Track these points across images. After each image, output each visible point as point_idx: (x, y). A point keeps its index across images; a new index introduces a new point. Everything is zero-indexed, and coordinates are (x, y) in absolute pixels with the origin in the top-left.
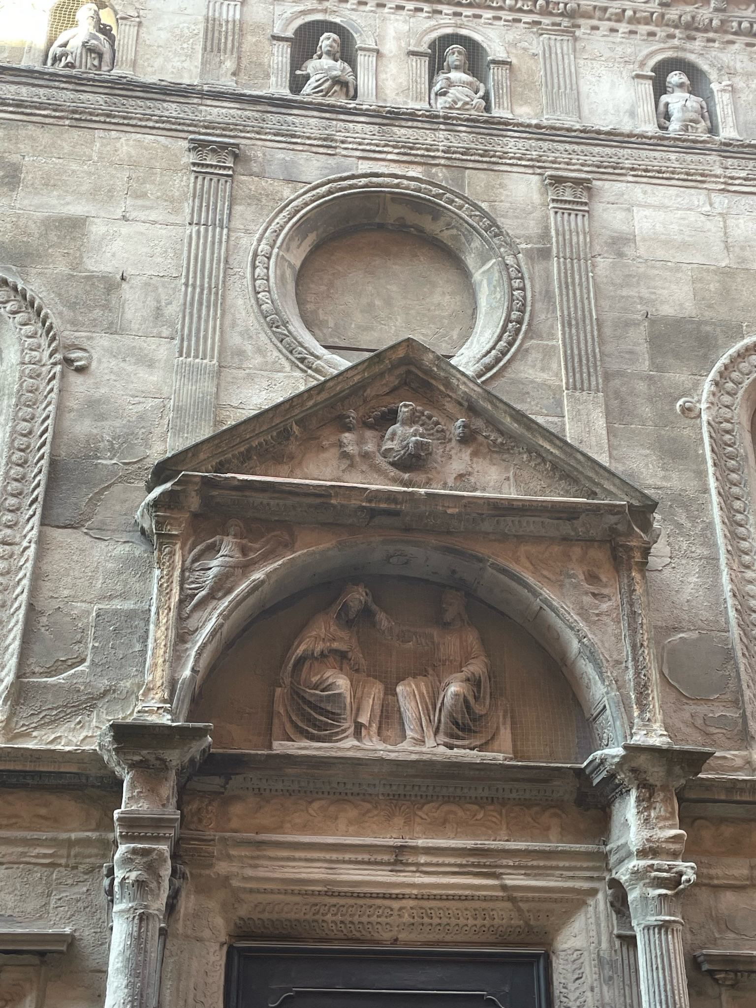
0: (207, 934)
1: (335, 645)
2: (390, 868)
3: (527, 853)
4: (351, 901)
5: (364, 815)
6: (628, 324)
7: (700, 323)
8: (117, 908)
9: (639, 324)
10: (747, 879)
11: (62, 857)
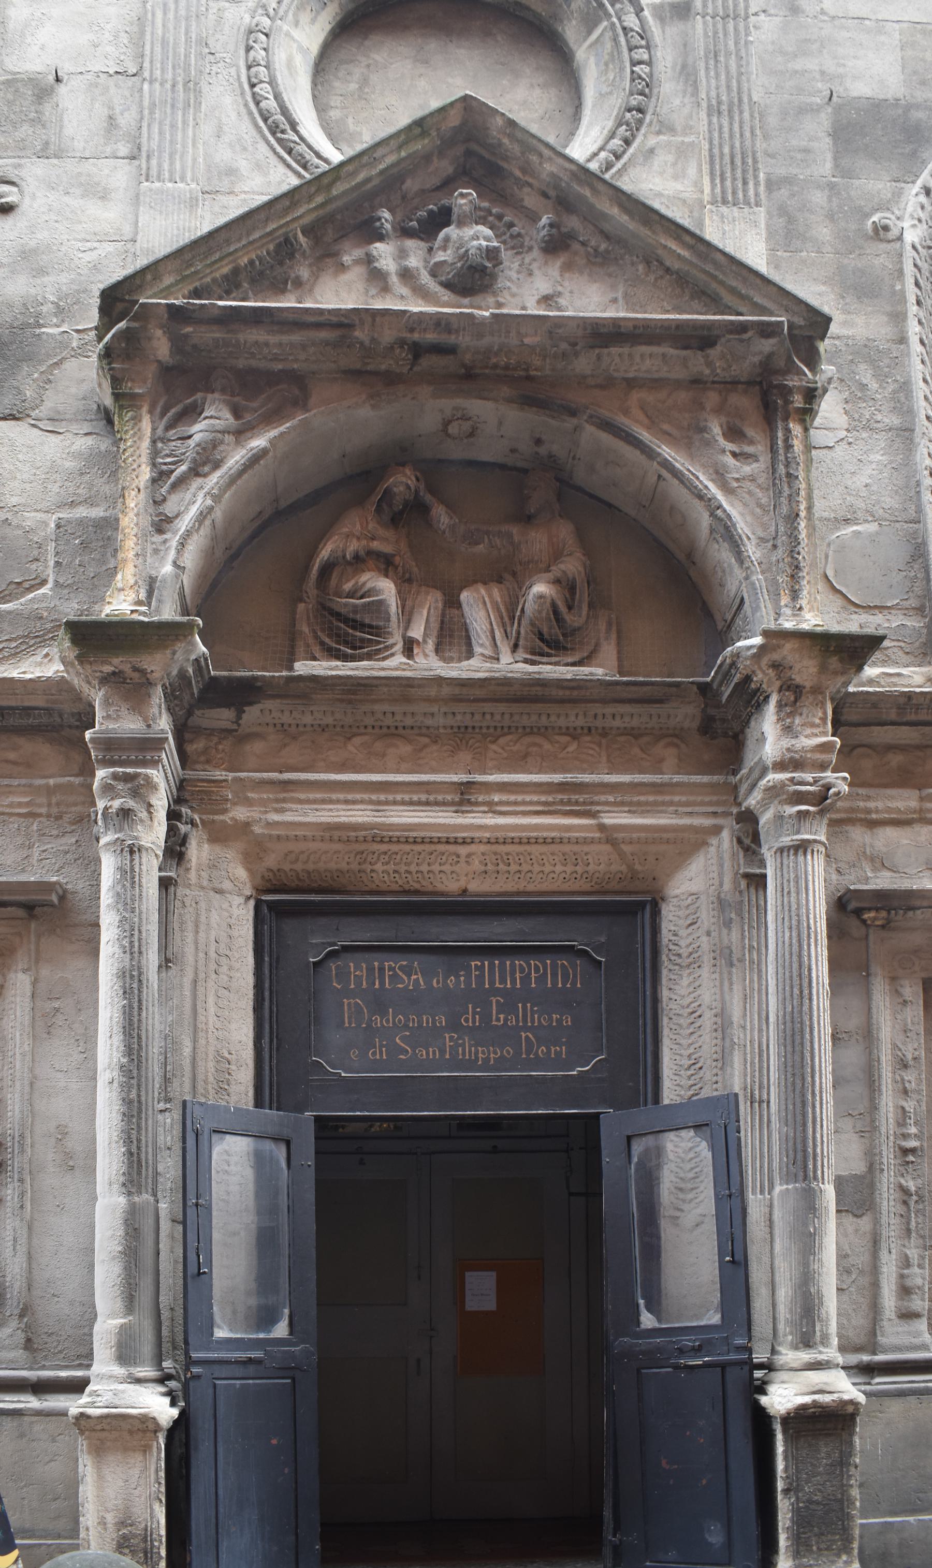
0: (227, 885)
1: (375, 545)
2: (454, 809)
3: (633, 786)
4: (407, 848)
5: (421, 750)
6: (804, 110)
7: (909, 107)
8: (103, 841)
9: (818, 111)
10: (915, 812)
11: (40, 806)
